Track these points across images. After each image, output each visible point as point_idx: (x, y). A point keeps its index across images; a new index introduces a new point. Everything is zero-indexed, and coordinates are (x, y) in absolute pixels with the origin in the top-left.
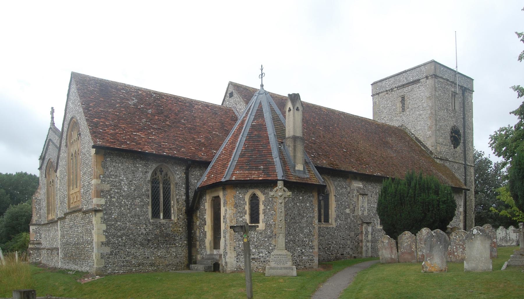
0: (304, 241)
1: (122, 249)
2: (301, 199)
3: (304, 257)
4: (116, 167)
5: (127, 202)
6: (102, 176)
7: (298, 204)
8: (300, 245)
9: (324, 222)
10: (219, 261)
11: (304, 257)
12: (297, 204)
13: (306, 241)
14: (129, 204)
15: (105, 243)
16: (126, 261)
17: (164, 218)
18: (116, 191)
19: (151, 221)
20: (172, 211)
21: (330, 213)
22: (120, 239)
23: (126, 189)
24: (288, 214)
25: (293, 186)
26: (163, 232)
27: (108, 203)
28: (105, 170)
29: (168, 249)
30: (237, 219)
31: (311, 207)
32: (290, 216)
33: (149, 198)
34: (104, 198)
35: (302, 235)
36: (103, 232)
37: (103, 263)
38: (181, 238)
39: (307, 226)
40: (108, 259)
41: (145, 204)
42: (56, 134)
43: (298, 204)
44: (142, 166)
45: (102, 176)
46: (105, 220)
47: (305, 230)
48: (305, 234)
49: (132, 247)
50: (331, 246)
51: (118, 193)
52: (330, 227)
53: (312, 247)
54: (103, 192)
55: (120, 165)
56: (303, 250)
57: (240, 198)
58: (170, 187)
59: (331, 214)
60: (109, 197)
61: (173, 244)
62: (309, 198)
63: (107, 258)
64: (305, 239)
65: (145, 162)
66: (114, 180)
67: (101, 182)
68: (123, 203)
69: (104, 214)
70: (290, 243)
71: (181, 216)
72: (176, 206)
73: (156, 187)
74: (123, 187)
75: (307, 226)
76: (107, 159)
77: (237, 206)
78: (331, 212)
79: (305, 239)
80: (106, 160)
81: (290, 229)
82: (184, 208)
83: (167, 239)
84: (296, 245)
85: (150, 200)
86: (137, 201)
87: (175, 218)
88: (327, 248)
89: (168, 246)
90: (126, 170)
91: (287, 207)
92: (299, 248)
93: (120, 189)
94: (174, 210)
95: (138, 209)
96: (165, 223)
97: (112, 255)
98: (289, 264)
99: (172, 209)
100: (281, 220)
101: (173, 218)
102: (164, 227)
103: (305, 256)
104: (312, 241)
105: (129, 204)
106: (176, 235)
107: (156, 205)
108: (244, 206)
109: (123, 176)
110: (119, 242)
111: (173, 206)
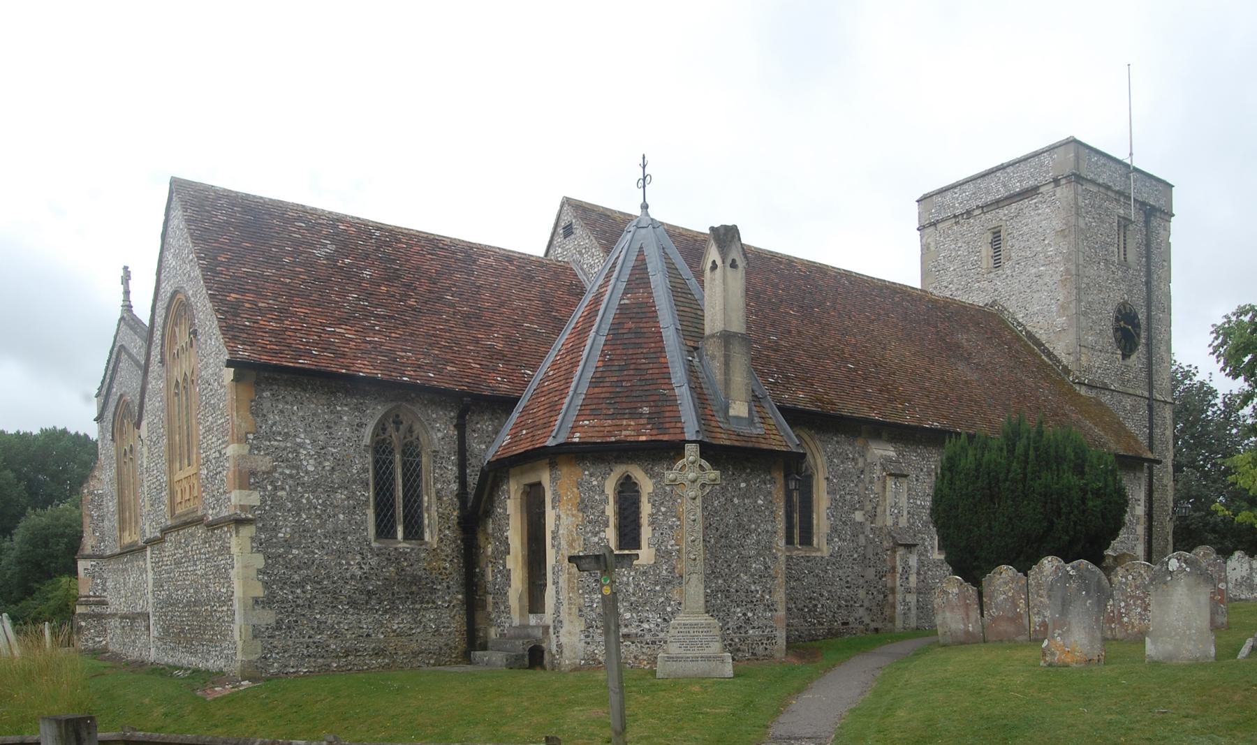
0: (752, 592)
1: (303, 615)
3: (751, 632)
9: (800, 544)
11: (751, 632)
13: (757, 591)
14: (319, 504)
15: (262, 602)
17: (406, 538)
18: (287, 472)
19: (374, 545)
22: (299, 591)
23: (311, 468)
24: (710, 525)
26: (403, 573)
28: (259, 420)
29: (417, 614)
32: (717, 530)
33: (369, 489)
35: (745, 578)
36: (258, 574)
37: (260, 651)
38: (448, 588)
45: (251, 436)
46: (261, 544)
47: (754, 565)
48: (752, 575)
51: (291, 476)
52: (815, 557)
53: (770, 607)
55: (295, 408)
56: (750, 614)
57: (593, 486)
58: (421, 461)
60: (269, 488)
61: (428, 602)
62: (763, 487)
63: (269, 637)
64: (753, 588)
67: (250, 451)
68: (304, 501)
69: (260, 530)
71: (447, 532)
74: (305, 463)
76: (264, 394)
82: (455, 514)
83: (414, 588)
84: (732, 601)
85: (371, 494)
89: (418, 606)
91: (710, 508)
92: (739, 610)
93: (297, 468)
96: (409, 550)
97: (281, 629)
100: (693, 541)
101: (427, 537)
102: (405, 559)
103: (754, 628)
104: (770, 592)
105: (319, 504)
109: (302, 436)
111: (428, 509)
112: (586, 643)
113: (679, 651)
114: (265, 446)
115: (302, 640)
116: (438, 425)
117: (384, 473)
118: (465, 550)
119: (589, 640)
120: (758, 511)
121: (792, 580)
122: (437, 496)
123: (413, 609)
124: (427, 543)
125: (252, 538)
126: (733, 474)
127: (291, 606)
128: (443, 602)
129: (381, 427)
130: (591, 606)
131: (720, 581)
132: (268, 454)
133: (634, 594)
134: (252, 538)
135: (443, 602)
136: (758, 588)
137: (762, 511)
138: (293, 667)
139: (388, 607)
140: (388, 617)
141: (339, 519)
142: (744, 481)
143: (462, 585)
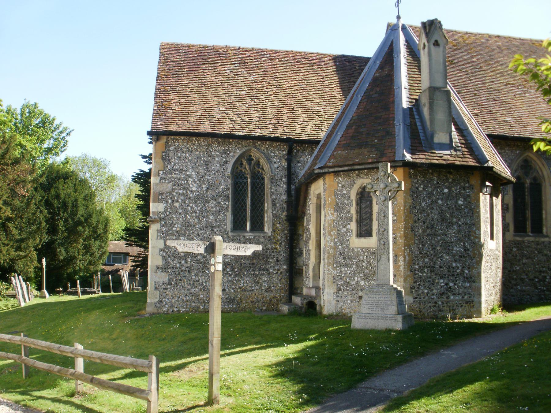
0: (453, 268)
1: (185, 276)
2: (445, 193)
3: (452, 297)
4: (182, 158)
5: (196, 208)
6: (161, 172)
7: (440, 202)
8: (445, 275)
9: (532, 232)
10: (316, 299)
12: (437, 202)
13: (458, 268)
14: (198, 210)
15: (161, 268)
16: (191, 293)
17: (252, 229)
18: (181, 192)
19: (230, 234)
20: (266, 219)
21: (544, 216)
22: (183, 262)
23: (195, 189)
24: (419, 219)
25: (430, 171)
27: (169, 210)
28: (166, 163)
29: (256, 277)
30: (338, 230)
31: (466, 207)
32: (424, 223)
33: (229, 200)
34: (163, 202)
35: (448, 258)
36: (160, 252)
37: (158, 297)
38: (278, 261)
39: (460, 240)
40: (165, 291)
41: (222, 209)
42: (350, 121)
43: (440, 202)
44: (220, 153)
45: (161, 172)
46: (163, 234)
47: (455, 248)
49: (200, 274)
50: (545, 274)
51: (183, 194)
52: (543, 242)
54: (162, 194)
55: (188, 155)
56: (451, 284)
57: (344, 194)
58: (264, 182)
59: (546, 218)
60: (170, 201)
61: (264, 270)
62: (463, 191)
63: (164, 289)
64: (454, 265)
65: (224, 147)
66: (179, 176)
67: (160, 180)
68: (189, 208)
69: (163, 226)
70: (422, 272)
71: (278, 225)
72: (270, 211)
73: (241, 184)
74: (191, 186)
75: (460, 240)
76: (171, 149)
77: (339, 207)
78: (546, 214)
79: (454, 265)
80: (168, 150)
81: (423, 245)
82: (284, 214)
83: (255, 261)
84: (436, 274)
85: (230, 203)
86: (210, 205)
87: (268, 230)
88: (538, 278)
90: (196, 161)
91: (418, 207)
92: (442, 281)
93: (187, 189)
94: (268, 217)
95: (211, 217)
97: (172, 284)
98: (391, 310)
99: (266, 215)
101: (266, 229)
105: (198, 210)
106: (270, 255)
107: (240, 210)
108: (349, 208)
109: (190, 170)
110: (182, 266)
111: (267, 212)
112: (336, 301)
113: (367, 311)
114: (169, 177)
115: (183, 291)
116: (275, 160)
117: (241, 190)
118: (290, 238)
119: (339, 299)
120: (459, 209)
121: (524, 258)
122: (272, 203)
123: (253, 274)
124: (265, 233)
125: (158, 230)
126: (438, 183)
127: (178, 271)
128: (274, 270)
129: (238, 162)
130: (341, 276)
131: (427, 260)
132: (170, 182)
133: (366, 268)
134: (158, 230)
135: (274, 270)
136: (458, 265)
137: (462, 209)
138: (176, 308)
139: (237, 273)
140: (237, 278)
141: (209, 218)
142: (446, 188)
143: (287, 259)
